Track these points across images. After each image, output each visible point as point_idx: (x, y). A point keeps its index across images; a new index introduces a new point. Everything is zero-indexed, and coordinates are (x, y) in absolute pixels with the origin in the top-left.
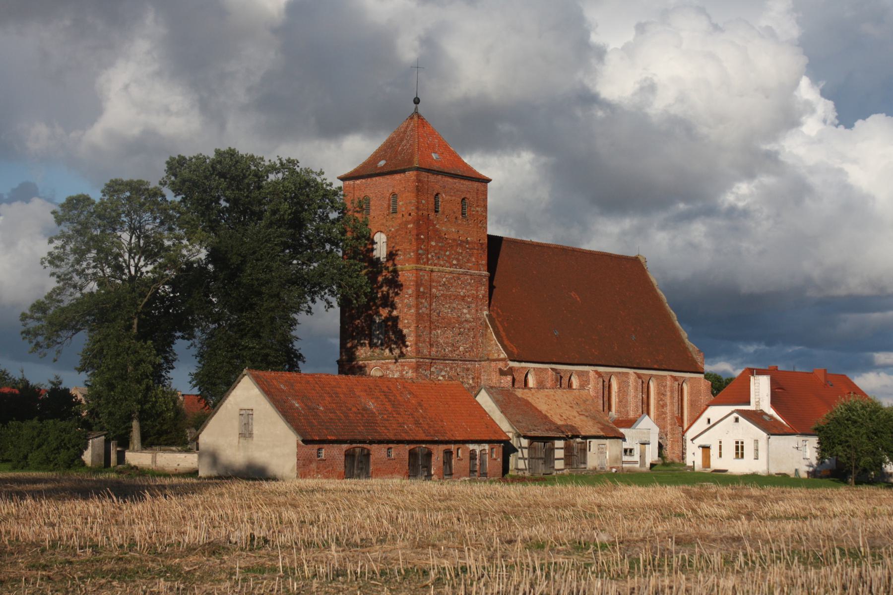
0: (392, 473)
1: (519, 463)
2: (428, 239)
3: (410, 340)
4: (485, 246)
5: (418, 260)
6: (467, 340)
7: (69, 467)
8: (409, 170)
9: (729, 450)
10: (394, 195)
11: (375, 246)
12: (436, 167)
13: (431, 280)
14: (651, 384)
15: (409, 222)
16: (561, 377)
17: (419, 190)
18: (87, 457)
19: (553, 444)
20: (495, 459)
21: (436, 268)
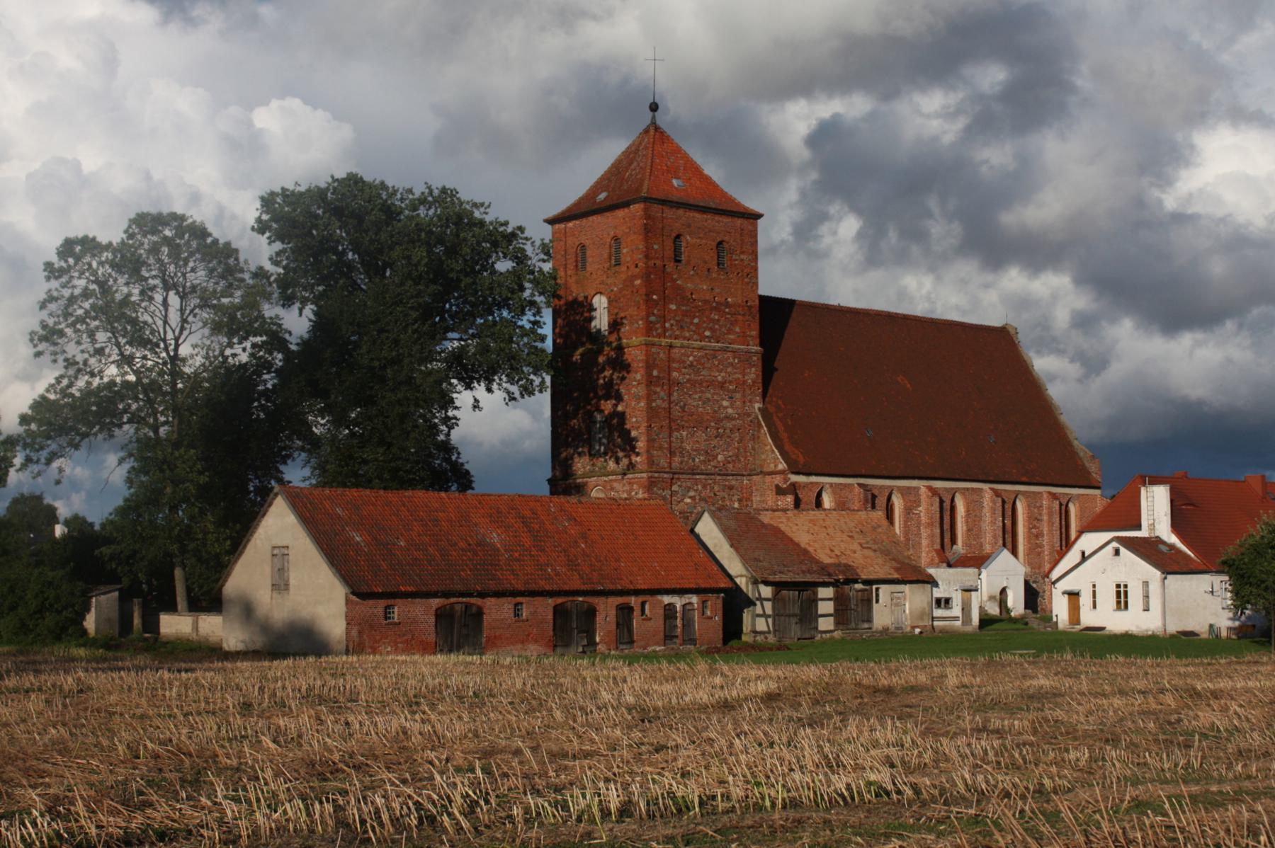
0: (523, 642)
1: (757, 622)
2: (665, 300)
3: (641, 445)
4: (755, 311)
5: (649, 330)
6: (729, 445)
7: (58, 638)
8: (634, 202)
9: (1107, 598)
10: (616, 239)
11: (594, 314)
12: (675, 197)
13: (670, 359)
14: (1019, 505)
15: (634, 277)
16: (874, 497)
17: (648, 232)
18: (90, 623)
19: (816, 594)
20: (710, 618)
21: (677, 342)
